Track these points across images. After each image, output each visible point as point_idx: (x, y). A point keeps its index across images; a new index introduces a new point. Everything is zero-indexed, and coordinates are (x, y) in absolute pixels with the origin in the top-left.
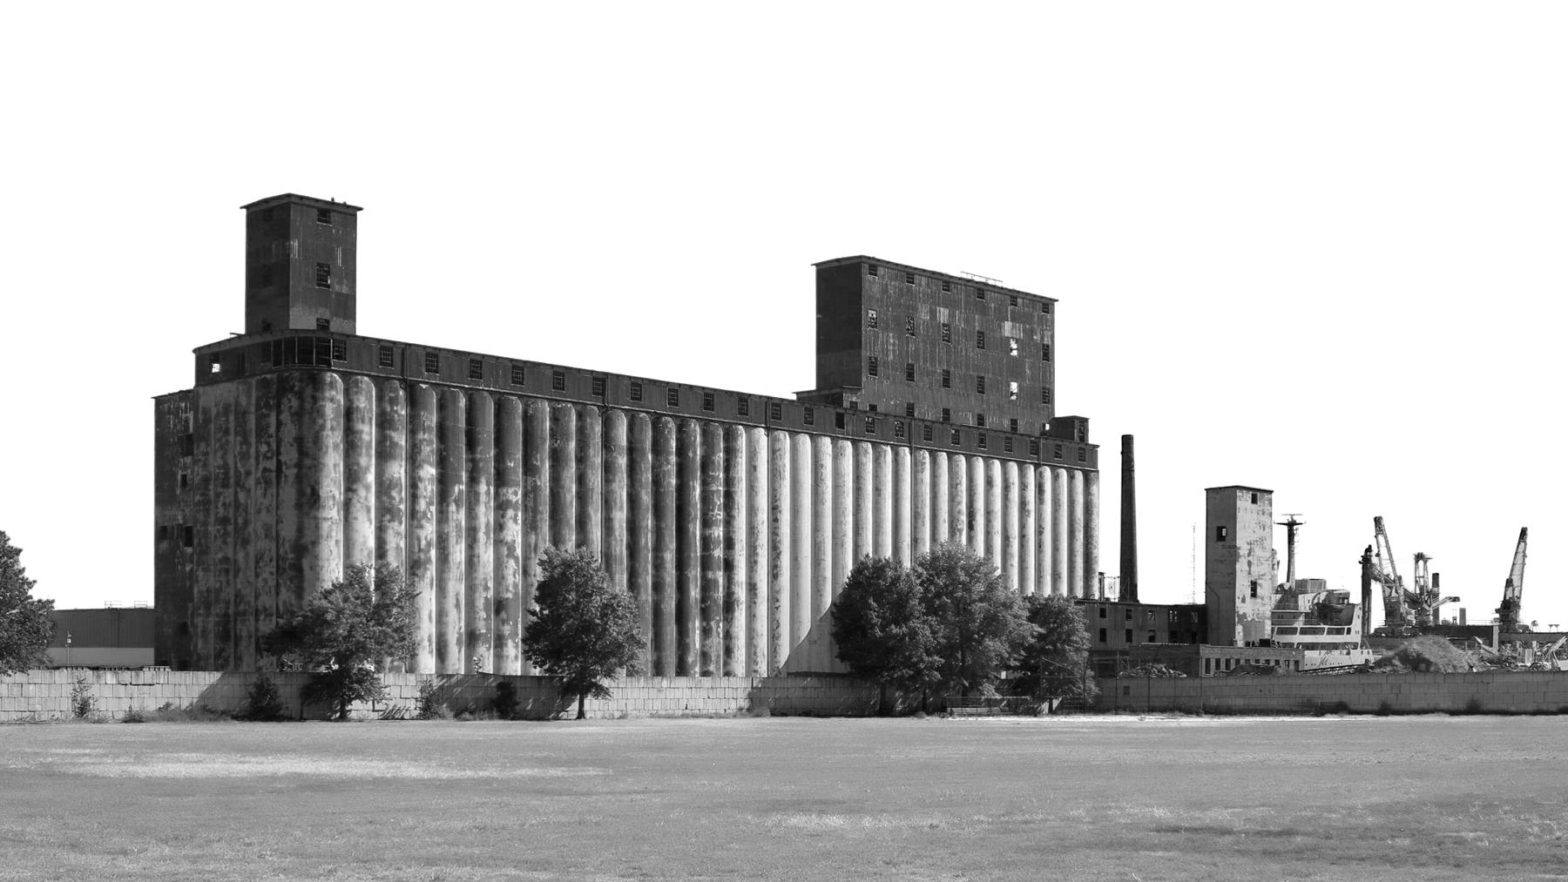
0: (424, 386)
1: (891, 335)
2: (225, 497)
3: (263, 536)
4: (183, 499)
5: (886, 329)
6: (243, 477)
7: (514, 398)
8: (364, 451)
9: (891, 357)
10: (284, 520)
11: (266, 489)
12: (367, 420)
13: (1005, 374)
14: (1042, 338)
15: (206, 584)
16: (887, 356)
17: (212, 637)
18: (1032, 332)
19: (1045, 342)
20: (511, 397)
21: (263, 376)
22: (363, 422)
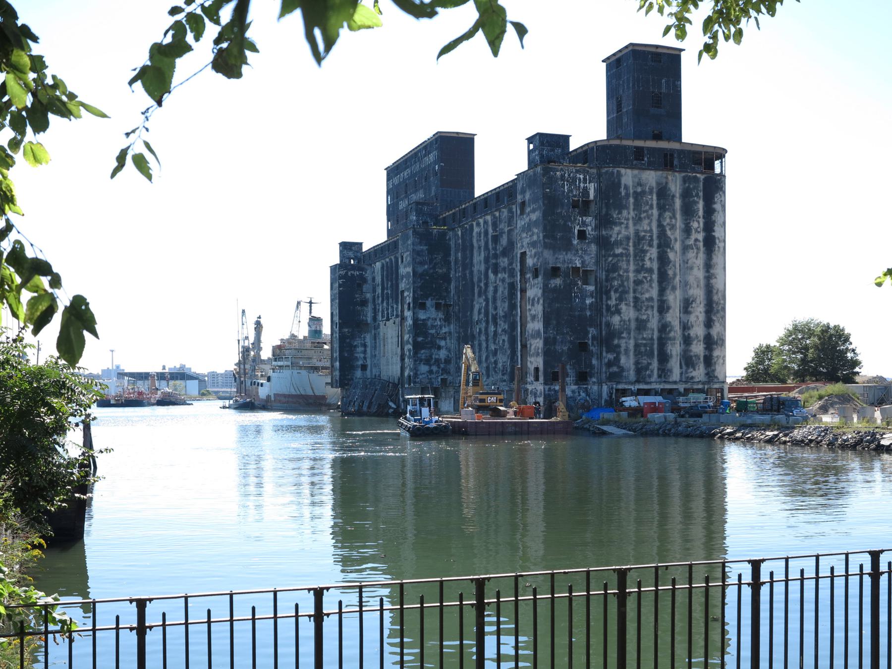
2: (651, 254)
3: (696, 286)
4: (582, 248)
6: (673, 242)
10: (717, 276)
11: (697, 253)
15: (628, 315)
17: (632, 354)
21: (694, 174)
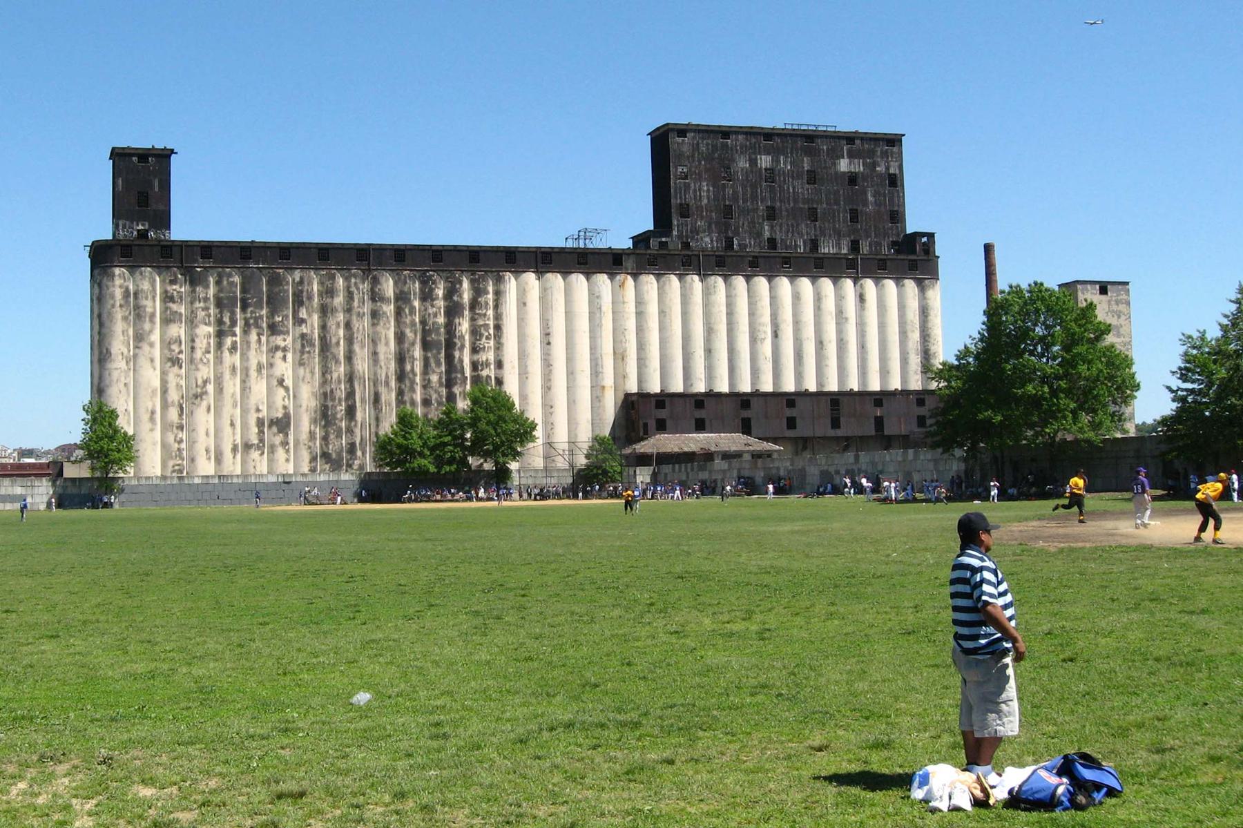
0: (199, 269)
1: (705, 184)
5: (700, 178)
7: (281, 271)
8: (147, 319)
9: (705, 201)
12: (150, 297)
13: (842, 203)
14: (888, 168)
16: (700, 200)
18: (875, 165)
19: (892, 171)
20: (278, 271)
22: (147, 298)
